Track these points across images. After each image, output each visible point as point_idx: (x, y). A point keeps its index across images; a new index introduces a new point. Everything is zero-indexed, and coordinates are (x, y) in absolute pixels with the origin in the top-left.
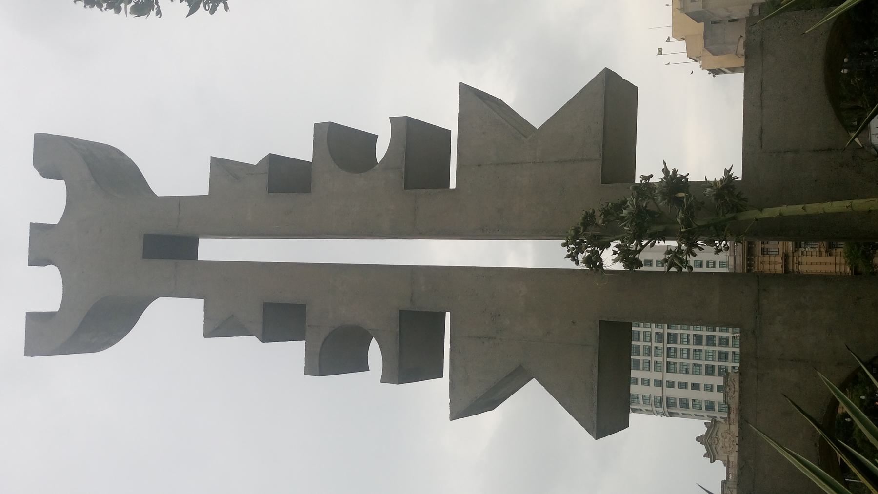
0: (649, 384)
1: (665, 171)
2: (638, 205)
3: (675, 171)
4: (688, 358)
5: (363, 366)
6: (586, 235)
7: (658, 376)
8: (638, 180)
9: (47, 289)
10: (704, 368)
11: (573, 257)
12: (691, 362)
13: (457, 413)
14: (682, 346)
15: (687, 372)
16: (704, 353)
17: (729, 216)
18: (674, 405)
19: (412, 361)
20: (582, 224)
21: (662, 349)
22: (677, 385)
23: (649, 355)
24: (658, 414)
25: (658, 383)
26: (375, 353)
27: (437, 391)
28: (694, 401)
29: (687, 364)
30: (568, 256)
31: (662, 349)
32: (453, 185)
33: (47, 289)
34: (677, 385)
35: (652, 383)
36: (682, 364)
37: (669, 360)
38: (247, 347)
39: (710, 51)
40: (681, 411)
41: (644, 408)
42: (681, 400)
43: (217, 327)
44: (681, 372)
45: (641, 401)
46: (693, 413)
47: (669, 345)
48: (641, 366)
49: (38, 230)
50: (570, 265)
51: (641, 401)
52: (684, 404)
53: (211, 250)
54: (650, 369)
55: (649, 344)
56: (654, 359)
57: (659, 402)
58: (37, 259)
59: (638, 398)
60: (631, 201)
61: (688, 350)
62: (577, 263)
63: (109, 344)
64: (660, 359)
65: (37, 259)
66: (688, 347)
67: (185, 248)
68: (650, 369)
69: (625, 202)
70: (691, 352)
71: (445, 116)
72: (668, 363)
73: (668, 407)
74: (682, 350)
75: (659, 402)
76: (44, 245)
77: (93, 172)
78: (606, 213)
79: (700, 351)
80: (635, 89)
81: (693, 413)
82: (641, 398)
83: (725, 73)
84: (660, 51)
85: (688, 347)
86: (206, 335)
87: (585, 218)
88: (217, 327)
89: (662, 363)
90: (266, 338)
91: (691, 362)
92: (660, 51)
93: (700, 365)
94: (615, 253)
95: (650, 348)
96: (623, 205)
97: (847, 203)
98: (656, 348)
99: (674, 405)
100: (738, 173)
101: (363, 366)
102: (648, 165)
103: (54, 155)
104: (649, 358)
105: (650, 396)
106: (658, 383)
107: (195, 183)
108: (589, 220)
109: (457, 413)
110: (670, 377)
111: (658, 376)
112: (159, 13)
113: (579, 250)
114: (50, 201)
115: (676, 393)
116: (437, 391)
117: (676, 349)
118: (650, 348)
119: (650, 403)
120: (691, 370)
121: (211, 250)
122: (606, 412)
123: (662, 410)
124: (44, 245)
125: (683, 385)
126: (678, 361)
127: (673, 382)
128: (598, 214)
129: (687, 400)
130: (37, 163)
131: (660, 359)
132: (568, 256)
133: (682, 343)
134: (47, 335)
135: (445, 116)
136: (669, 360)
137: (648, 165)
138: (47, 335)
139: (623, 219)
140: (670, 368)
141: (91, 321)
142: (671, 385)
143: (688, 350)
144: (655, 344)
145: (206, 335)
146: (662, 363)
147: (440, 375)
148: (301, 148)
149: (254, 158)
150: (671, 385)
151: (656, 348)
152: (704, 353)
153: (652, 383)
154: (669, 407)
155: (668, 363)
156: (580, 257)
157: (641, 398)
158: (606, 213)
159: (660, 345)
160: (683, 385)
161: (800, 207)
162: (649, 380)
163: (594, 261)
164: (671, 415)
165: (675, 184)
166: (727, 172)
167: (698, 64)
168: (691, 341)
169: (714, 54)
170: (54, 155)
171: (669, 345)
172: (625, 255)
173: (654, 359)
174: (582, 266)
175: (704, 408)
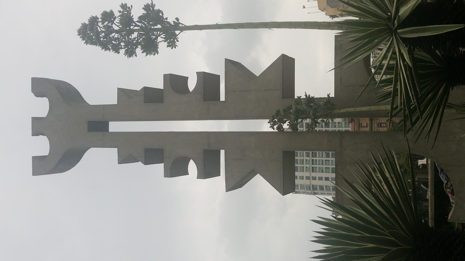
0: (303, 179)
1: (306, 95)
2: (296, 108)
3: (309, 95)
4: (323, 164)
5: (186, 173)
6: (276, 118)
7: (307, 174)
8: (296, 97)
9: (42, 146)
10: (331, 169)
11: (272, 127)
12: (324, 166)
13: (229, 188)
14: (320, 159)
15: (322, 172)
16: (330, 162)
17: (329, 112)
18: (316, 189)
19: (208, 170)
20: (276, 115)
21: (309, 160)
22: (317, 178)
23: (303, 164)
24: (308, 194)
25: (308, 178)
26: (192, 167)
27: (219, 182)
28: (326, 186)
29: (322, 168)
30: (270, 127)
31: (309, 160)
32: (222, 98)
33: (42, 146)
34: (317, 178)
35: (305, 178)
36: (319, 168)
37: (313, 166)
38: (138, 166)
39: (330, 6)
40: (320, 192)
41: (301, 191)
42: (320, 186)
43: (123, 159)
44: (319, 172)
45: (299, 188)
46: (326, 193)
47: (313, 158)
48: (299, 170)
49: (35, 120)
50: (271, 130)
51: (299, 188)
52: (321, 188)
53: (115, 127)
54: (303, 171)
55: (303, 158)
56: (305, 166)
57: (308, 188)
58: (35, 133)
59: (298, 186)
60: (294, 107)
61: (323, 160)
62: (274, 129)
63: (69, 169)
64: (308, 166)
65: (35, 133)
66: (322, 159)
67: (104, 126)
68: (303, 171)
69: (291, 106)
70: (324, 161)
71: (219, 70)
72: (313, 167)
73: (313, 190)
74: (319, 160)
75: (308, 188)
76: (38, 126)
77: (60, 94)
78: (285, 111)
79: (329, 160)
80: (294, 60)
81: (326, 193)
82: (299, 186)
83: (338, 17)
84: (304, 7)
85: (322, 159)
86: (120, 163)
87: (277, 112)
88: (123, 159)
89: (310, 168)
90: (146, 163)
91: (324, 166)
92: (304, 7)
93: (329, 168)
94: (288, 125)
95: (303, 160)
96: (290, 108)
97: (369, 107)
98: (306, 160)
99: (316, 189)
100: (332, 95)
101: (186, 173)
102: (300, 91)
103: (40, 87)
104: (303, 165)
105: (304, 185)
106: (308, 178)
107: (112, 99)
108: (278, 113)
109: (229, 188)
110: (314, 174)
111: (307, 174)
112: (136, 55)
113: (274, 125)
114: (42, 107)
115: (317, 183)
116: (219, 182)
117: (316, 160)
118: (303, 160)
119: (304, 189)
120: (324, 171)
121: (115, 127)
122: (287, 185)
123: (310, 191)
124: (38, 126)
125: (321, 179)
126: (318, 166)
127: (316, 177)
128: (281, 111)
129: (323, 186)
130: (33, 91)
131: (308, 166)
132: (270, 127)
133: (319, 157)
134: (41, 166)
135: (219, 70)
136: (313, 166)
137: (300, 91)
138: (41, 166)
139: (291, 113)
140: (313, 170)
141: (61, 160)
142: (314, 178)
143: (323, 160)
144: (305, 158)
145: (120, 163)
146: (310, 168)
147: (219, 175)
148: (159, 84)
149: (138, 88)
150: (314, 178)
151: (306, 160)
152: (330, 162)
153: (305, 178)
154: (313, 190)
155: (313, 167)
156: (275, 127)
157: (299, 186)
158: (285, 111)
159: (308, 158)
160: (321, 179)
161: (353, 109)
162: (303, 177)
163: (280, 128)
164: (315, 194)
165: (310, 100)
166: (328, 95)
167: (324, 13)
168: (324, 156)
169: (332, 8)
170: (40, 87)
171: (313, 158)
172: (291, 126)
173: (305, 166)
174: (276, 130)
175: (331, 190)
